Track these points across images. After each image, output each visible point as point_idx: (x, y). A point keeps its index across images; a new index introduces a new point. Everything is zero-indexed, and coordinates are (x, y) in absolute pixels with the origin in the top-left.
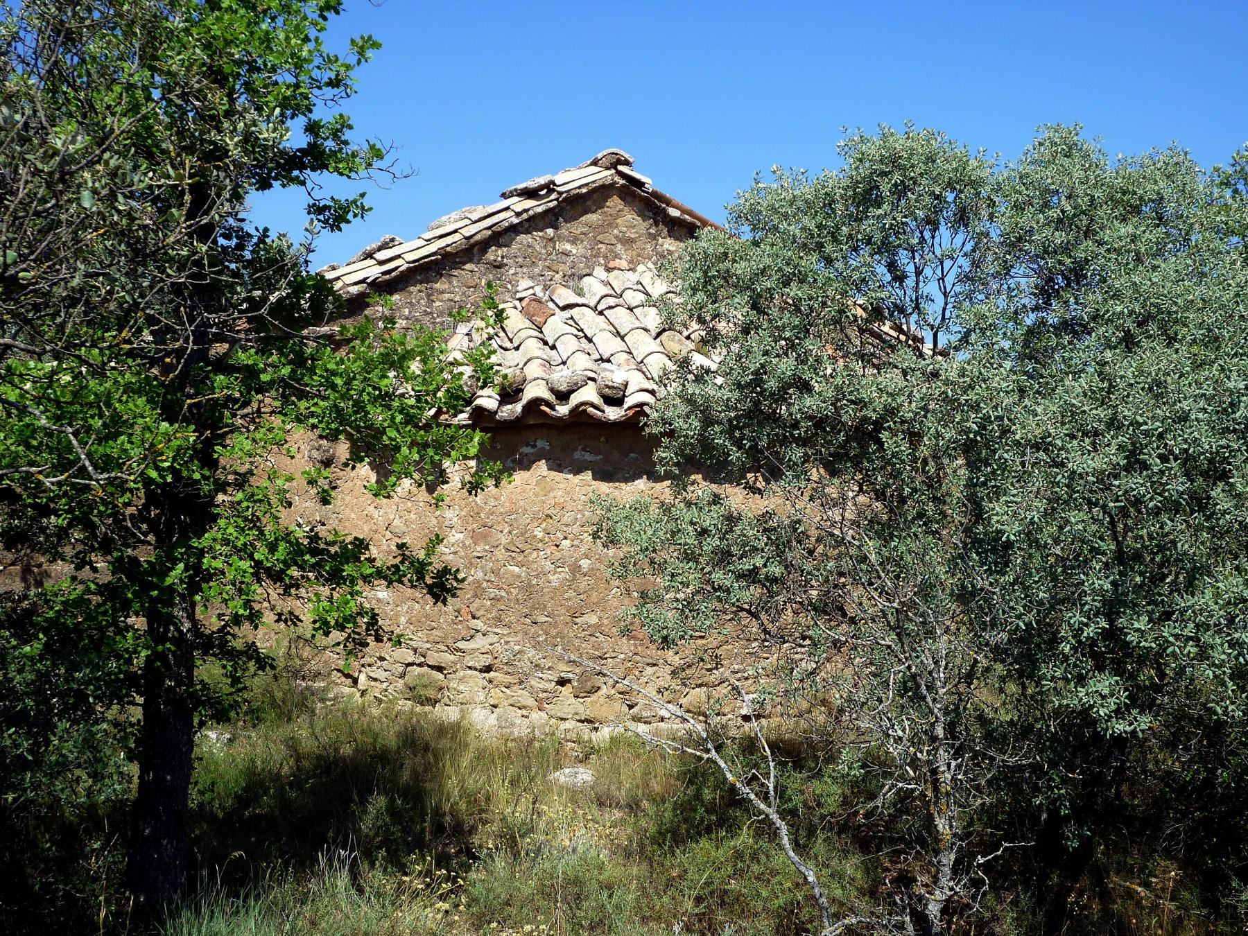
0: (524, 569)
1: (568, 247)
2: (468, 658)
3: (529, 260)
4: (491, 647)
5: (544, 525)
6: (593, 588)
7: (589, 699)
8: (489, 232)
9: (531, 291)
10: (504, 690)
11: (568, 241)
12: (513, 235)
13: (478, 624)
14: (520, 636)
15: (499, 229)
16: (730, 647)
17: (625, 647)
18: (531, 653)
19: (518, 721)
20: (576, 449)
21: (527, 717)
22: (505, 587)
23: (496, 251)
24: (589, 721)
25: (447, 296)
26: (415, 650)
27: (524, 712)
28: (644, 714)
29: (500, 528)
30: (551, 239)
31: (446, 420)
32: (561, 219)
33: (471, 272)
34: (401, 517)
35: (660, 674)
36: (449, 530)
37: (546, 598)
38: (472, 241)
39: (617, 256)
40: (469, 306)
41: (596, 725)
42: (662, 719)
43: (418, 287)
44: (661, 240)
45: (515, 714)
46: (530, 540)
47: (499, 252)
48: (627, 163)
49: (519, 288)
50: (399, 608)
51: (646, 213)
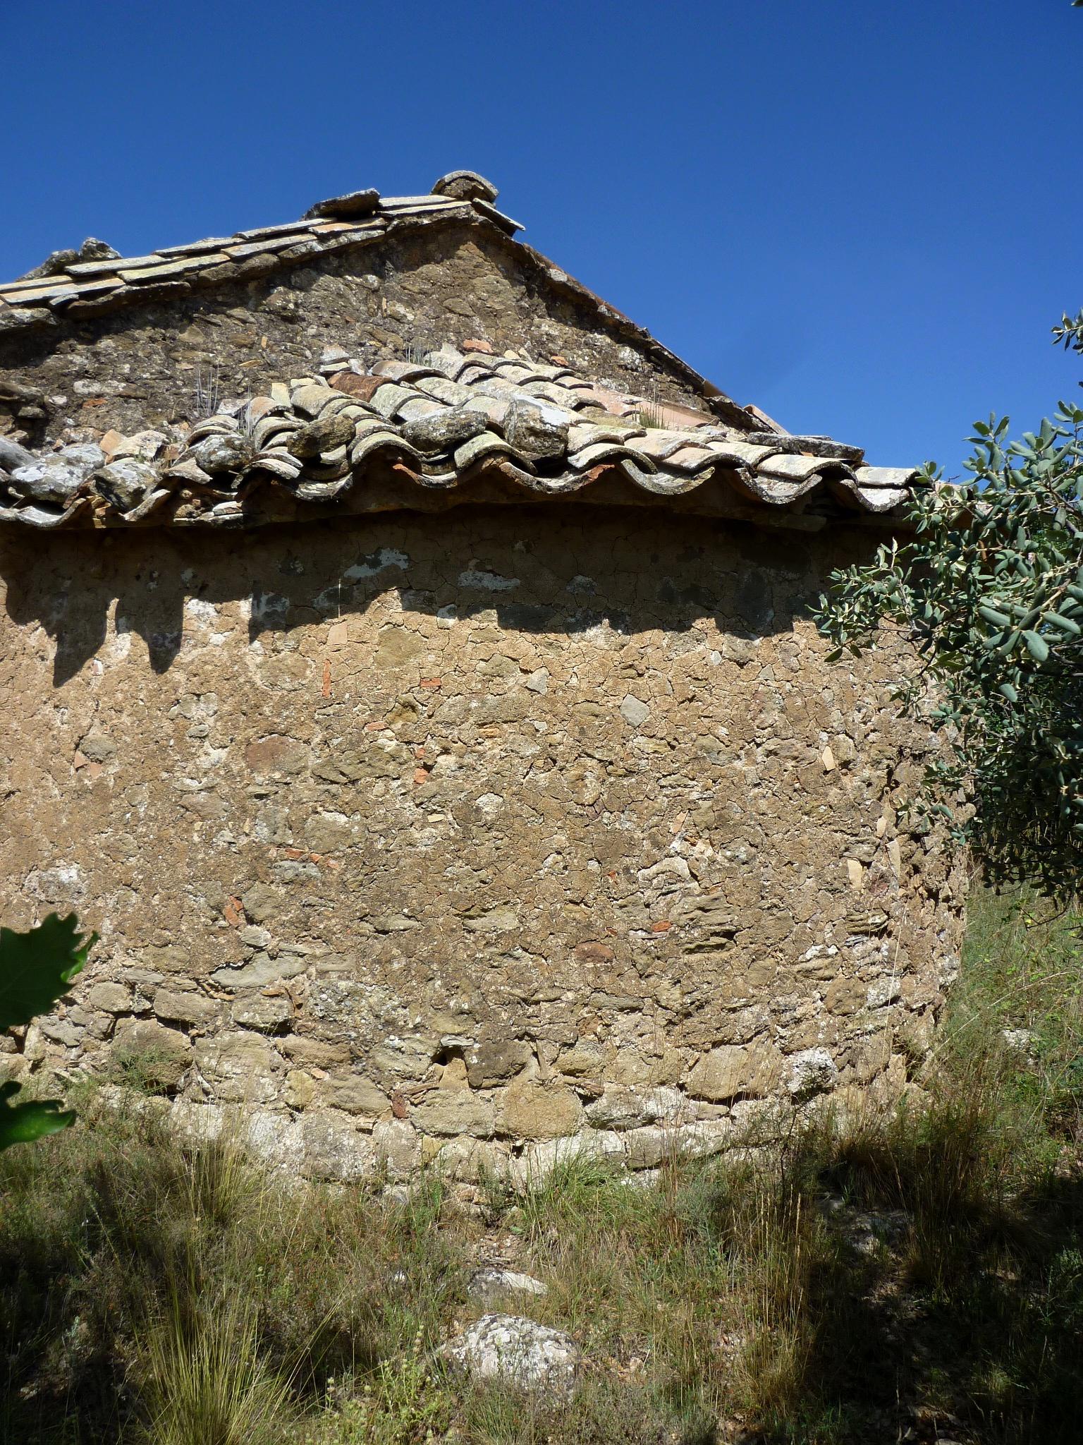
0: (358, 817)
1: (401, 309)
2: (238, 1005)
3: (339, 320)
4: (288, 984)
5: (398, 725)
6: (507, 856)
7: (504, 1091)
8: (274, 259)
9: (344, 365)
10: (319, 1073)
11: (400, 301)
12: (314, 274)
13: (262, 934)
14: (350, 960)
15: (291, 256)
16: (769, 962)
17: (575, 977)
18: (375, 996)
19: (348, 1141)
20: (463, 566)
21: (370, 1132)
22: (317, 857)
23: (286, 293)
24: (500, 1136)
25: (201, 355)
26: (132, 986)
27: (362, 1121)
28: (616, 1113)
29: (304, 734)
30: (375, 291)
31: (190, 515)
32: (389, 265)
33: (244, 322)
34: (103, 722)
35: (645, 1028)
36: (197, 742)
37: (407, 879)
38: (246, 266)
39: (474, 334)
40: (240, 376)
41: (518, 1144)
42: (651, 1120)
43: (149, 331)
44: (537, 320)
45: (342, 1127)
46: (369, 757)
47: (291, 296)
48: (488, 196)
49: (325, 358)
50: (99, 903)
51: (516, 276)
